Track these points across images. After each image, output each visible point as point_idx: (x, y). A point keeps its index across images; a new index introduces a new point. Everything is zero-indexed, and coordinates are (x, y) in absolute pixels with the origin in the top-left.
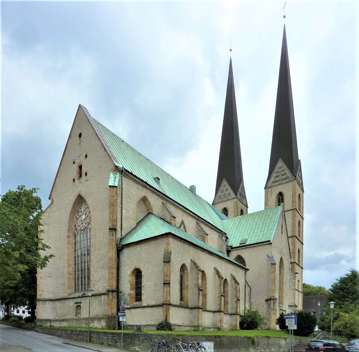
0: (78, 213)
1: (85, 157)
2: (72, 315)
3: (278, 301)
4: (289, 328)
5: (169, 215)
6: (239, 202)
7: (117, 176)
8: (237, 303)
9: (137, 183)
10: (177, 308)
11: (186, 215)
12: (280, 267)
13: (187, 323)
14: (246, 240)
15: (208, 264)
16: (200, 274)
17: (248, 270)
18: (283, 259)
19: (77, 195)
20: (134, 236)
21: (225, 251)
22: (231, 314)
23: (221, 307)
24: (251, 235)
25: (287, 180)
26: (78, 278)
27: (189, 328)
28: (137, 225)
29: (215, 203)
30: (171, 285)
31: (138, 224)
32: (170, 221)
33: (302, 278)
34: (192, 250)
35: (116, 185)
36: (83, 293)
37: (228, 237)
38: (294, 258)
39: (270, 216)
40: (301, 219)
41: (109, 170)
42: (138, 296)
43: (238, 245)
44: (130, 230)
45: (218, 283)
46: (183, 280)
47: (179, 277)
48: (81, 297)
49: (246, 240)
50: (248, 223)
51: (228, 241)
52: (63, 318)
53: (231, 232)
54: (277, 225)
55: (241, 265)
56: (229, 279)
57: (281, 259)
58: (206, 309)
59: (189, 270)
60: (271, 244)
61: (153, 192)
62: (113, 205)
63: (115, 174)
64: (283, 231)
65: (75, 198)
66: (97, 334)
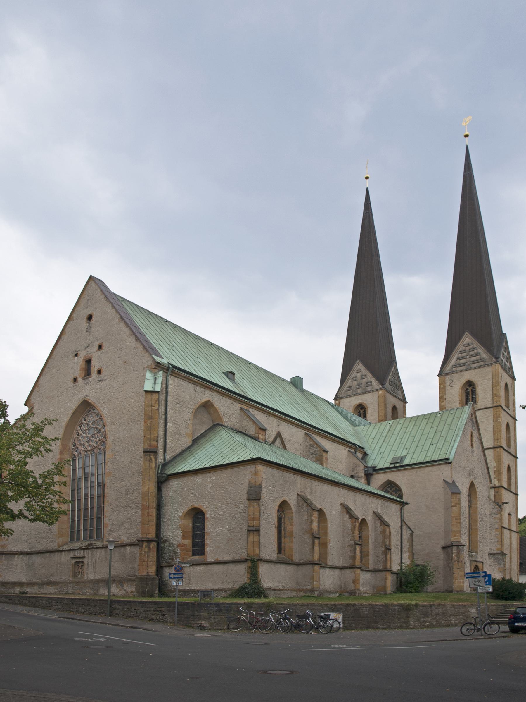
0: (80, 427)
1: (97, 348)
2: (66, 577)
3: (466, 549)
5: (254, 426)
6: (388, 395)
7: (159, 376)
8: (386, 554)
9: (194, 383)
10: (273, 564)
12: (470, 496)
13: (290, 585)
14: (403, 458)
15: (329, 500)
16: (316, 514)
17: (407, 504)
18: (476, 484)
19: (81, 401)
20: (189, 461)
22: (375, 571)
23: (354, 561)
24: (412, 450)
25: (482, 363)
26: (79, 521)
27: (294, 593)
28: (193, 443)
29: (341, 396)
30: (262, 533)
31: (195, 441)
32: (256, 435)
33: (517, 509)
34: (299, 480)
35: (158, 388)
36: (87, 543)
37: (368, 452)
38: (499, 480)
40: (511, 421)
41: (144, 368)
42: (198, 546)
43: (387, 465)
44: (179, 450)
45: (349, 526)
46: (283, 524)
48: (84, 549)
49: (403, 458)
50: (407, 431)
51: (367, 459)
52: (48, 580)
53: (373, 446)
54: (462, 435)
55: (394, 497)
56: (369, 519)
57: (472, 485)
58: (327, 565)
59: (294, 510)
60: (450, 463)
61: (222, 394)
62: (151, 418)
63: (155, 374)
64: (473, 443)
66: (126, 605)
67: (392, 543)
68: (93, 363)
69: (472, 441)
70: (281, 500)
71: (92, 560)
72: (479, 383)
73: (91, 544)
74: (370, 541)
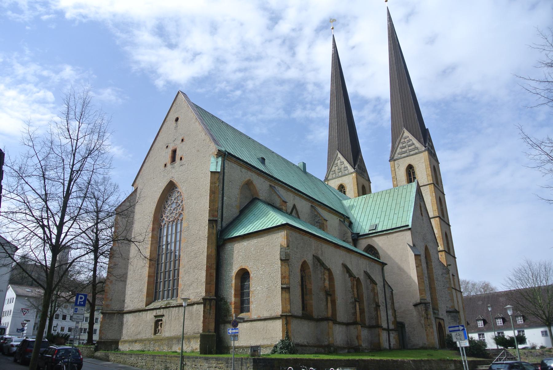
4: (458, 346)
5: (279, 199)
9: (303, 198)
11: (297, 198)
12: (426, 257)
17: (386, 264)
18: (429, 247)
21: (350, 240)
23: (356, 318)
24: (382, 219)
25: (417, 151)
32: (281, 207)
33: (457, 271)
35: (219, 170)
36: (166, 302)
39: (404, 195)
42: (243, 304)
44: (231, 219)
45: (350, 284)
47: (300, 278)
52: (136, 338)
56: (362, 277)
57: (426, 248)
59: (311, 269)
65: (166, 185)
66: (194, 361)
67: (380, 301)
68: (178, 152)
69: (421, 211)
70: (303, 261)
71: (169, 317)
72: (416, 166)
73: (169, 303)
74: (364, 299)
